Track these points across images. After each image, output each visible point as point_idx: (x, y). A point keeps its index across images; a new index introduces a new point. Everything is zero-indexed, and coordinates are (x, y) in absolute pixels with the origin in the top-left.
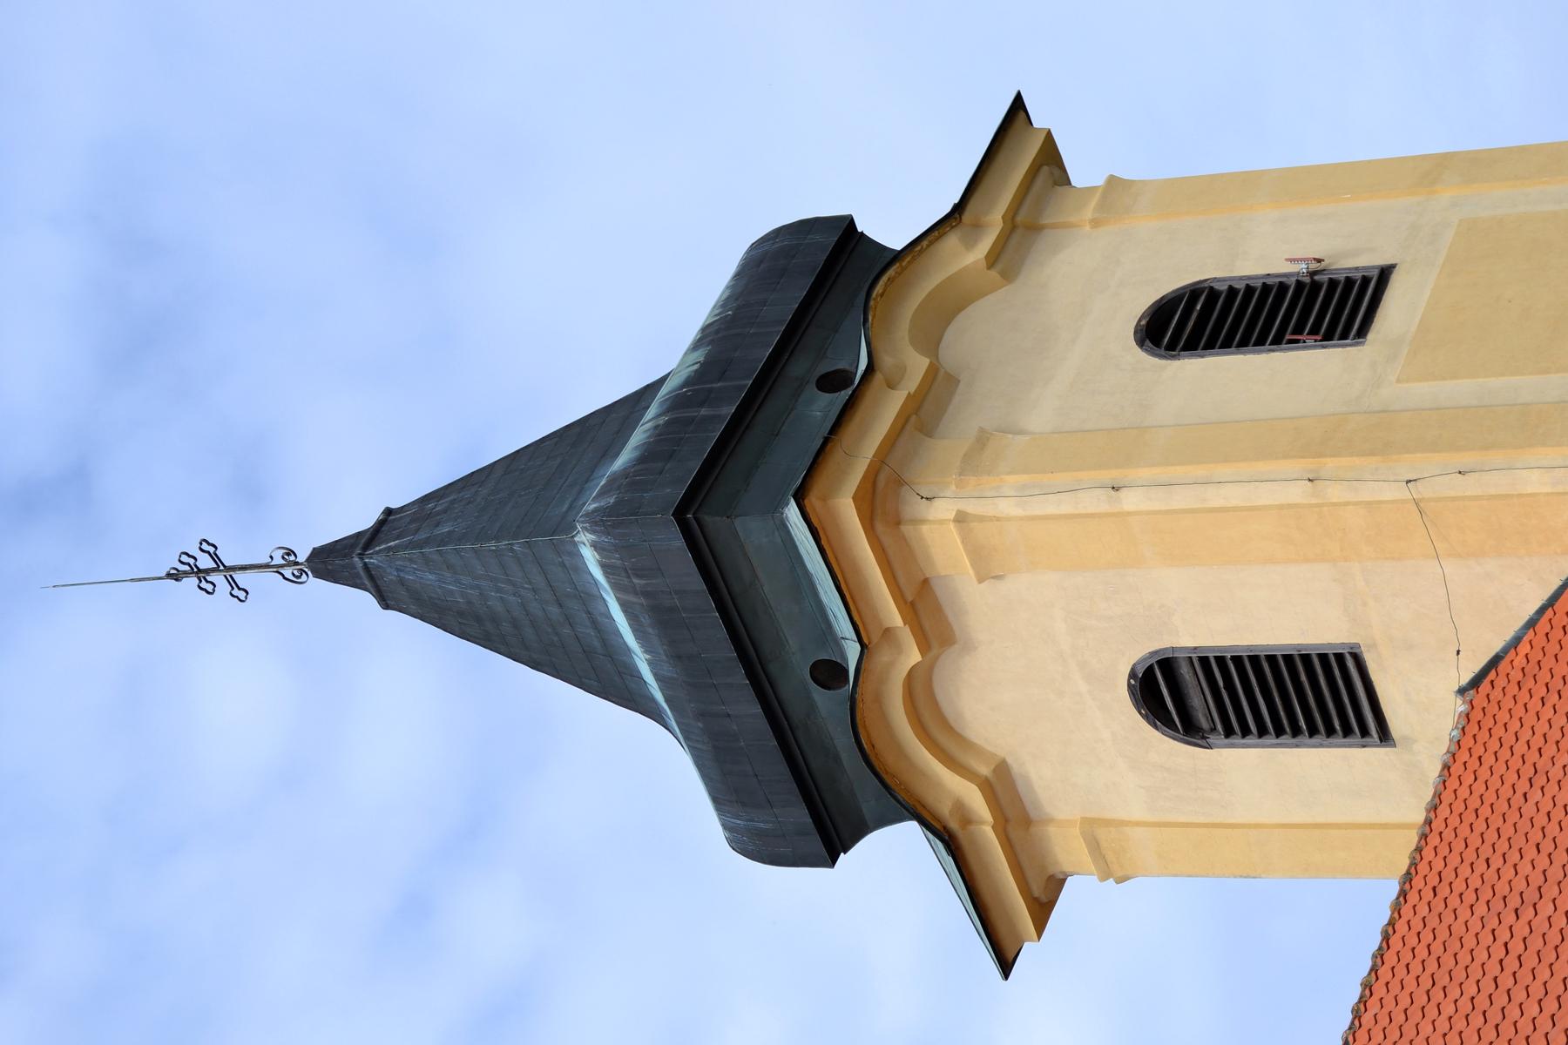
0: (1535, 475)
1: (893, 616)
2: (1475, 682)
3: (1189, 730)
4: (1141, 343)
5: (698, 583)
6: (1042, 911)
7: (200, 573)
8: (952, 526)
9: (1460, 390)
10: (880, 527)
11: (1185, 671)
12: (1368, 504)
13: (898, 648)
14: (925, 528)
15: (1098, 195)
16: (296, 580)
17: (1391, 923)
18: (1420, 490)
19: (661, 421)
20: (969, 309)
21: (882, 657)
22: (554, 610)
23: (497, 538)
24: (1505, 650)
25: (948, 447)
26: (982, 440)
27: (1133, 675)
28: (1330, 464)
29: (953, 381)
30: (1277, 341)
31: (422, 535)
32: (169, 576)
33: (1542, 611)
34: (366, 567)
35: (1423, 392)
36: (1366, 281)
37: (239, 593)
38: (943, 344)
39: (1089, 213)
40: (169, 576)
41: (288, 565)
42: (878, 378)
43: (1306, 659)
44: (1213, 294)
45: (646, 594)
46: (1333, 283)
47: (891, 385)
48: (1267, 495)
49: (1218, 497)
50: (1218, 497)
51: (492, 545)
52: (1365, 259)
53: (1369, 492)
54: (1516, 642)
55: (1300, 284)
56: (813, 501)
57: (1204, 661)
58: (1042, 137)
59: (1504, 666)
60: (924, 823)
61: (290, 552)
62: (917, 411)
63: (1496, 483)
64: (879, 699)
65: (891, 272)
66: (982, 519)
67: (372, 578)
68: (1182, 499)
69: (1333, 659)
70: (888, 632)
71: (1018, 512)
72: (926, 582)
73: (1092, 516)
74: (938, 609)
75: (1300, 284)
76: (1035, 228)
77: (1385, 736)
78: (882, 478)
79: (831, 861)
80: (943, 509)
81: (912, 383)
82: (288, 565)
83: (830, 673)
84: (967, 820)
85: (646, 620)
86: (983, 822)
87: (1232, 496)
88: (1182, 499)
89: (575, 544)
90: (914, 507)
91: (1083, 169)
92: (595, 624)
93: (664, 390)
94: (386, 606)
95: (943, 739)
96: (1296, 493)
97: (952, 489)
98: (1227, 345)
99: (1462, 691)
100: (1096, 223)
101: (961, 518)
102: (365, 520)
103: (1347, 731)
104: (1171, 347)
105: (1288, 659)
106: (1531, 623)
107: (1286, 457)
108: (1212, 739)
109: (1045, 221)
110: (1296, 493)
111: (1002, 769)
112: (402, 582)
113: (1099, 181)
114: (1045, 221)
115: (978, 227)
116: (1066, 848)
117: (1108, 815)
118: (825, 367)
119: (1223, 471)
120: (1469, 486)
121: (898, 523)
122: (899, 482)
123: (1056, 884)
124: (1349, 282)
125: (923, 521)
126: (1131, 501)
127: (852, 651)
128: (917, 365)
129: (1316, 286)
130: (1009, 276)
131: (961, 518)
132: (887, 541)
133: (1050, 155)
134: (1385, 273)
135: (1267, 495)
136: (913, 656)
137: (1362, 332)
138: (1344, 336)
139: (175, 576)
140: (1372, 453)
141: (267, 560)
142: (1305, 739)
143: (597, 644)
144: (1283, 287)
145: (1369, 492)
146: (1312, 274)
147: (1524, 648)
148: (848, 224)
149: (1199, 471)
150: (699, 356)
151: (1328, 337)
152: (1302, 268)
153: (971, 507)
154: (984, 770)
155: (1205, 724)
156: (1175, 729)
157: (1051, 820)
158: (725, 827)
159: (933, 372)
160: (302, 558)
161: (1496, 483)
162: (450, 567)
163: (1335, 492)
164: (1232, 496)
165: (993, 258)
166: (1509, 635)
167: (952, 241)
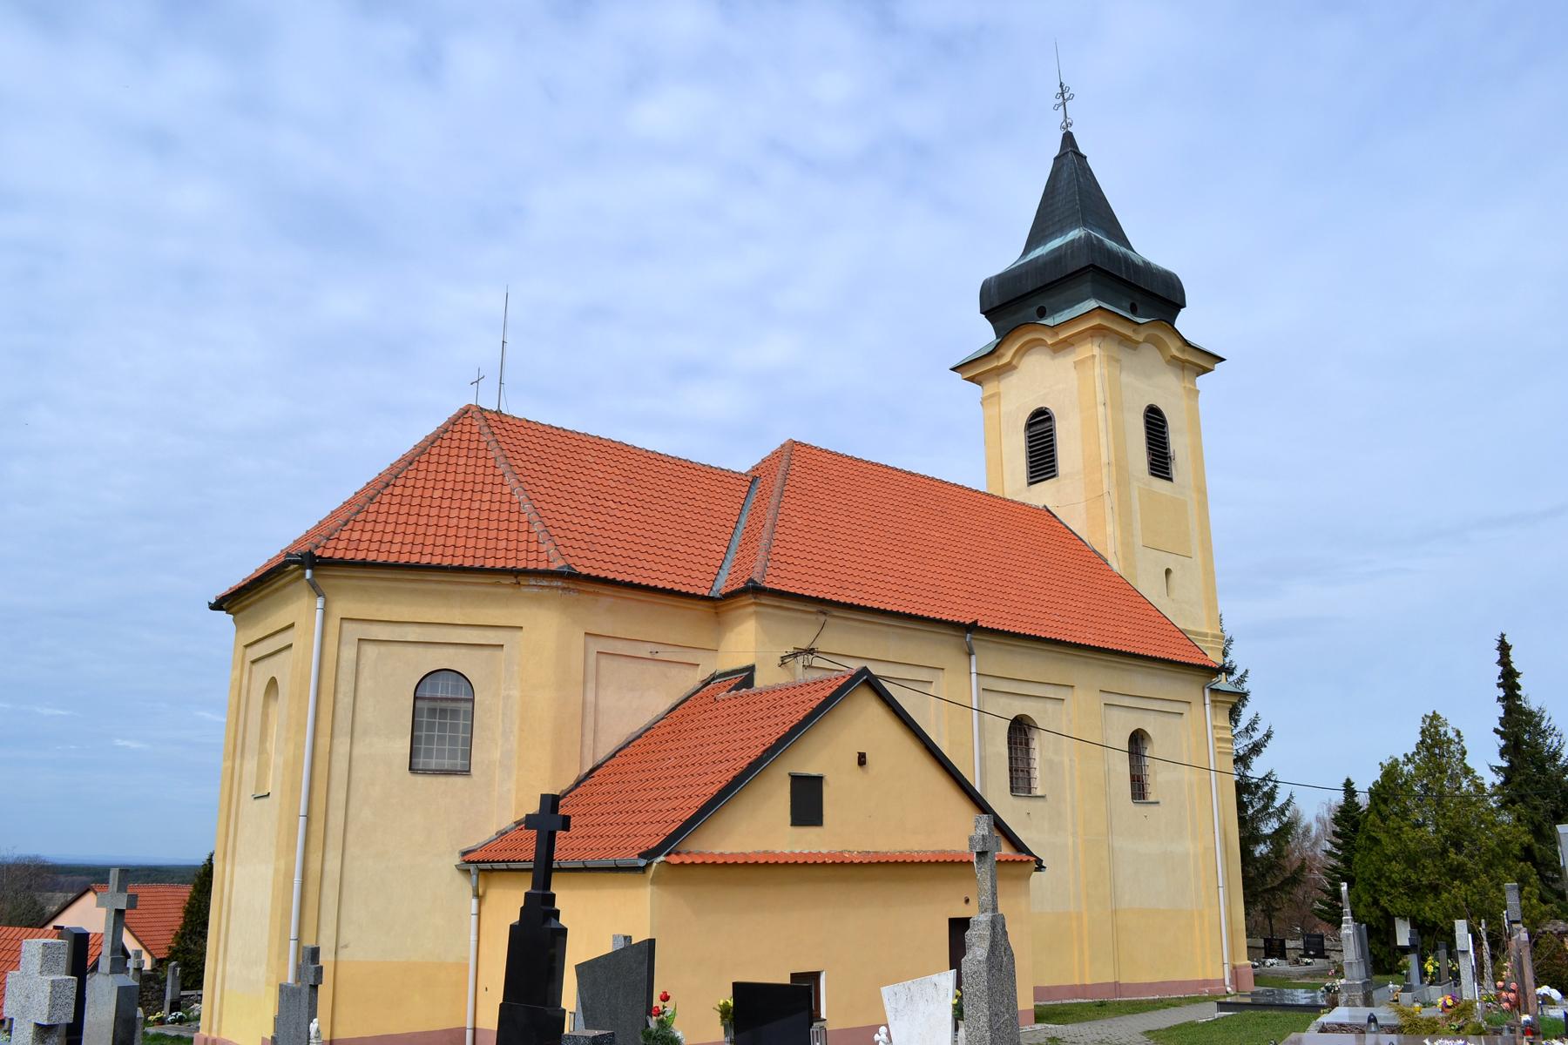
0: (1112, 529)
1: (1061, 336)
2: (1048, 511)
3: (1029, 425)
4: (1148, 407)
5: (1069, 272)
6: (971, 379)
7: (1062, 94)
8: (1091, 354)
9: (1136, 505)
10: (1091, 331)
11: (1048, 424)
12: (1102, 481)
13: (1052, 336)
14: (1090, 345)
15: (1192, 387)
16: (1062, 127)
17: (980, 492)
18: (1106, 496)
19: (1120, 255)
20: (1158, 351)
21: (1049, 331)
22: (1057, 219)
23: (1080, 199)
24: (1058, 519)
25: (1115, 350)
26: (1118, 361)
27: (1046, 408)
28: (1113, 469)
29: (1135, 349)
30: (1150, 448)
31: (1079, 171)
32: (1061, 83)
33: (1071, 530)
34: (1067, 153)
35: (1135, 494)
36: (1168, 474)
37: (1056, 108)
38: (1152, 346)
39: (1188, 385)
40: (1061, 83)
41: (1067, 124)
42: (1136, 327)
43: (1053, 461)
44: (1163, 427)
45: (1065, 254)
46: (1167, 464)
47: (1134, 331)
48: (1104, 450)
49: (1102, 435)
50: (1102, 435)
51: (1077, 198)
52: (1174, 473)
53: (1105, 481)
54: (1062, 523)
55: (1167, 453)
56: (1099, 311)
57: (1051, 430)
58: (1209, 367)
59: (1054, 519)
60: (998, 344)
61: (1071, 125)
62: (1127, 339)
63: (1109, 518)
64: (1036, 330)
65: (1168, 325)
66: (1094, 363)
67: (1064, 154)
68: (1102, 425)
69: (1051, 443)
70: (1057, 334)
71: (1096, 374)
72: (1073, 345)
73: (1096, 397)
74: (1064, 349)
75: (1167, 453)
76: (1183, 369)
77: (1030, 484)
78: (1104, 331)
79: (982, 313)
80: (1096, 351)
81: (1135, 337)
82: (1067, 124)
83: (1042, 313)
84: (999, 357)
85: (1056, 254)
86: (998, 362)
87: (1103, 440)
88: (1102, 425)
89: (1079, 227)
90: (1097, 341)
91: (1202, 380)
92: (1053, 233)
93: (1130, 252)
94: (1055, 159)
95: (1020, 353)
96: (1104, 459)
97: (1102, 353)
98: (1148, 433)
99: (1045, 506)
100: (1185, 387)
101: (1094, 356)
102: (1082, 150)
103: (1031, 473)
104: (1147, 416)
105: (1053, 455)
106: (1067, 527)
107: (1115, 455)
108: (1027, 432)
109: (1185, 372)
110: (1104, 459)
111: (1015, 368)
112: (1063, 165)
113: (1198, 388)
114: (1185, 372)
115: (1183, 351)
116: (991, 387)
117: (1002, 401)
118: (1138, 304)
119: (1111, 436)
120: (1108, 511)
121: (1091, 336)
122: (1104, 336)
123: (979, 383)
124: (1168, 469)
125: (1092, 345)
126: (1101, 409)
127: (1049, 321)
128: (1140, 338)
129: (1166, 458)
130: (1168, 362)
131: (1094, 356)
132: (1086, 333)
133: (1206, 370)
134: (1170, 479)
135: (1104, 450)
136: (1049, 342)
137: (1153, 474)
138: (1151, 469)
139: (1061, 86)
140: (1117, 481)
141: (1068, 116)
142: (1029, 460)
143: (1047, 233)
144: (1166, 448)
145: (1105, 481)
146: (1170, 457)
147: (1060, 525)
148: (1184, 306)
149: (1110, 429)
150: (1141, 263)
151: (1151, 464)
152: (1172, 454)
153: (1097, 360)
154: (1014, 363)
155: (1031, 430)
156: (1031, 419)
157: (999, 382)
158: (991, 278)
159: (1138, 343)
160: (1069, 129)
161: (1109, 518)
162: (1069, 183)
163: (1105, 471)
164: (1103, 440)
165: (1174, 357)
166: (1062, 520)
167: (1179, 344)
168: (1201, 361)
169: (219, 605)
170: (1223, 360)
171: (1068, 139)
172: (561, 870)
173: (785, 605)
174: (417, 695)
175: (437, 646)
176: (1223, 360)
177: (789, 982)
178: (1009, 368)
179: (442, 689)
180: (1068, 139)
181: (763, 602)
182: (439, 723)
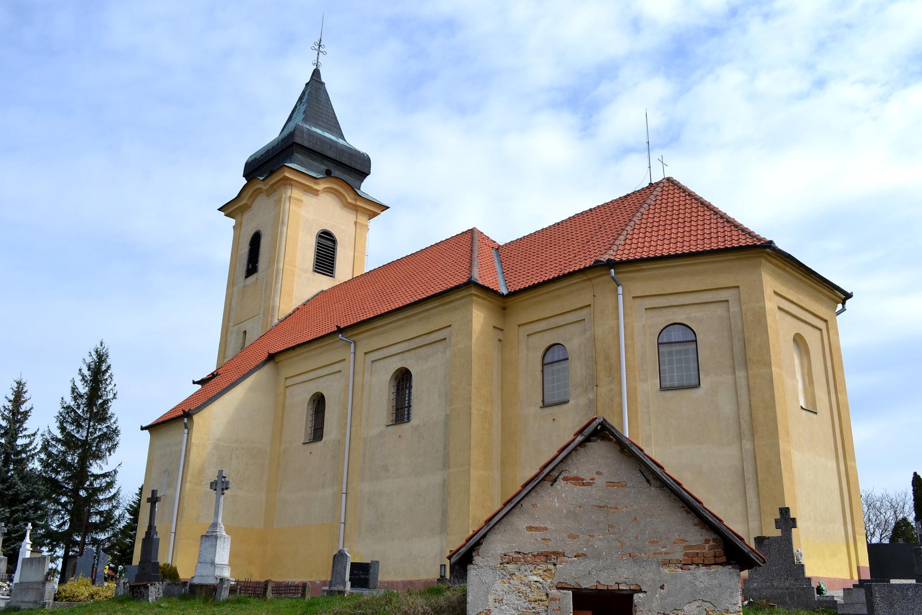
84: (315, 183)
111: (317, 195)
133: (375, 215)
137: (315, 271)
168: (376, 208)
169: (220, 209)
170: (388, 208)
171: (316, 73)
172: (762, 533)
173: (451, 299)
174: (659, 342)
175: (545, 290)
176: (388, 208)
177: (870, 579)
178: (315, 193)
179: (677, 334)
180: (316, 73)
181: (643, 267)
182: (683, 381)
